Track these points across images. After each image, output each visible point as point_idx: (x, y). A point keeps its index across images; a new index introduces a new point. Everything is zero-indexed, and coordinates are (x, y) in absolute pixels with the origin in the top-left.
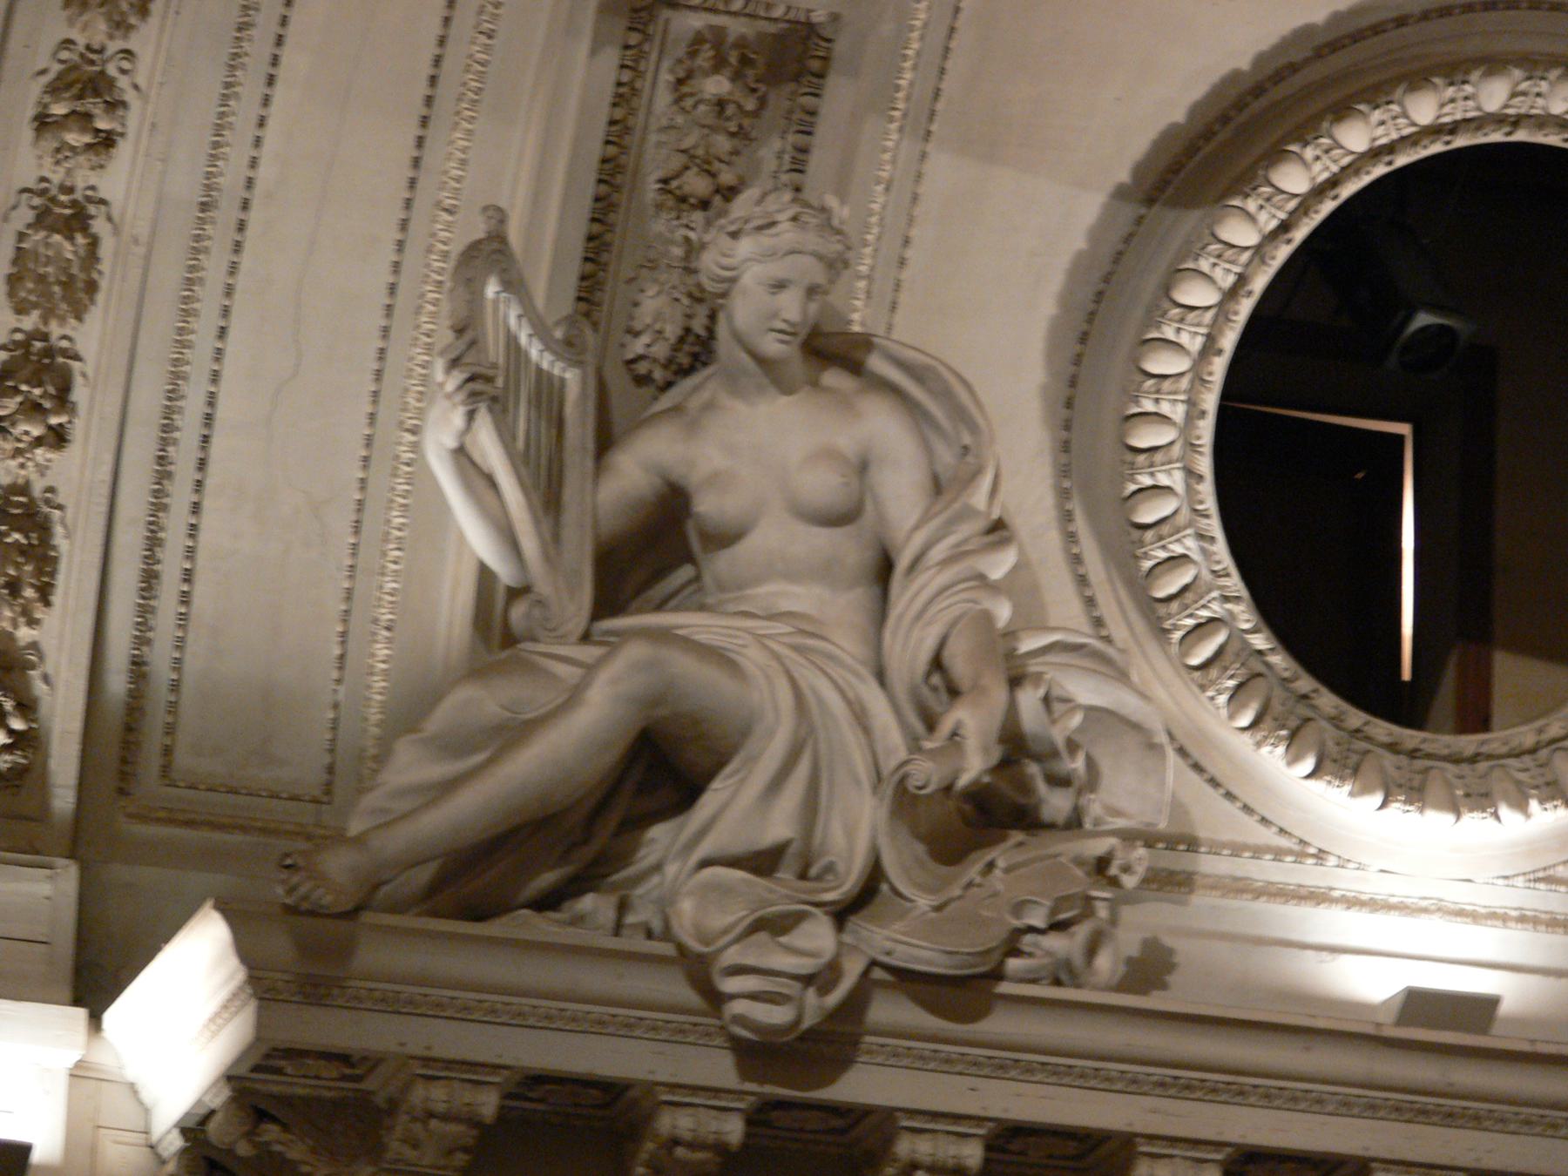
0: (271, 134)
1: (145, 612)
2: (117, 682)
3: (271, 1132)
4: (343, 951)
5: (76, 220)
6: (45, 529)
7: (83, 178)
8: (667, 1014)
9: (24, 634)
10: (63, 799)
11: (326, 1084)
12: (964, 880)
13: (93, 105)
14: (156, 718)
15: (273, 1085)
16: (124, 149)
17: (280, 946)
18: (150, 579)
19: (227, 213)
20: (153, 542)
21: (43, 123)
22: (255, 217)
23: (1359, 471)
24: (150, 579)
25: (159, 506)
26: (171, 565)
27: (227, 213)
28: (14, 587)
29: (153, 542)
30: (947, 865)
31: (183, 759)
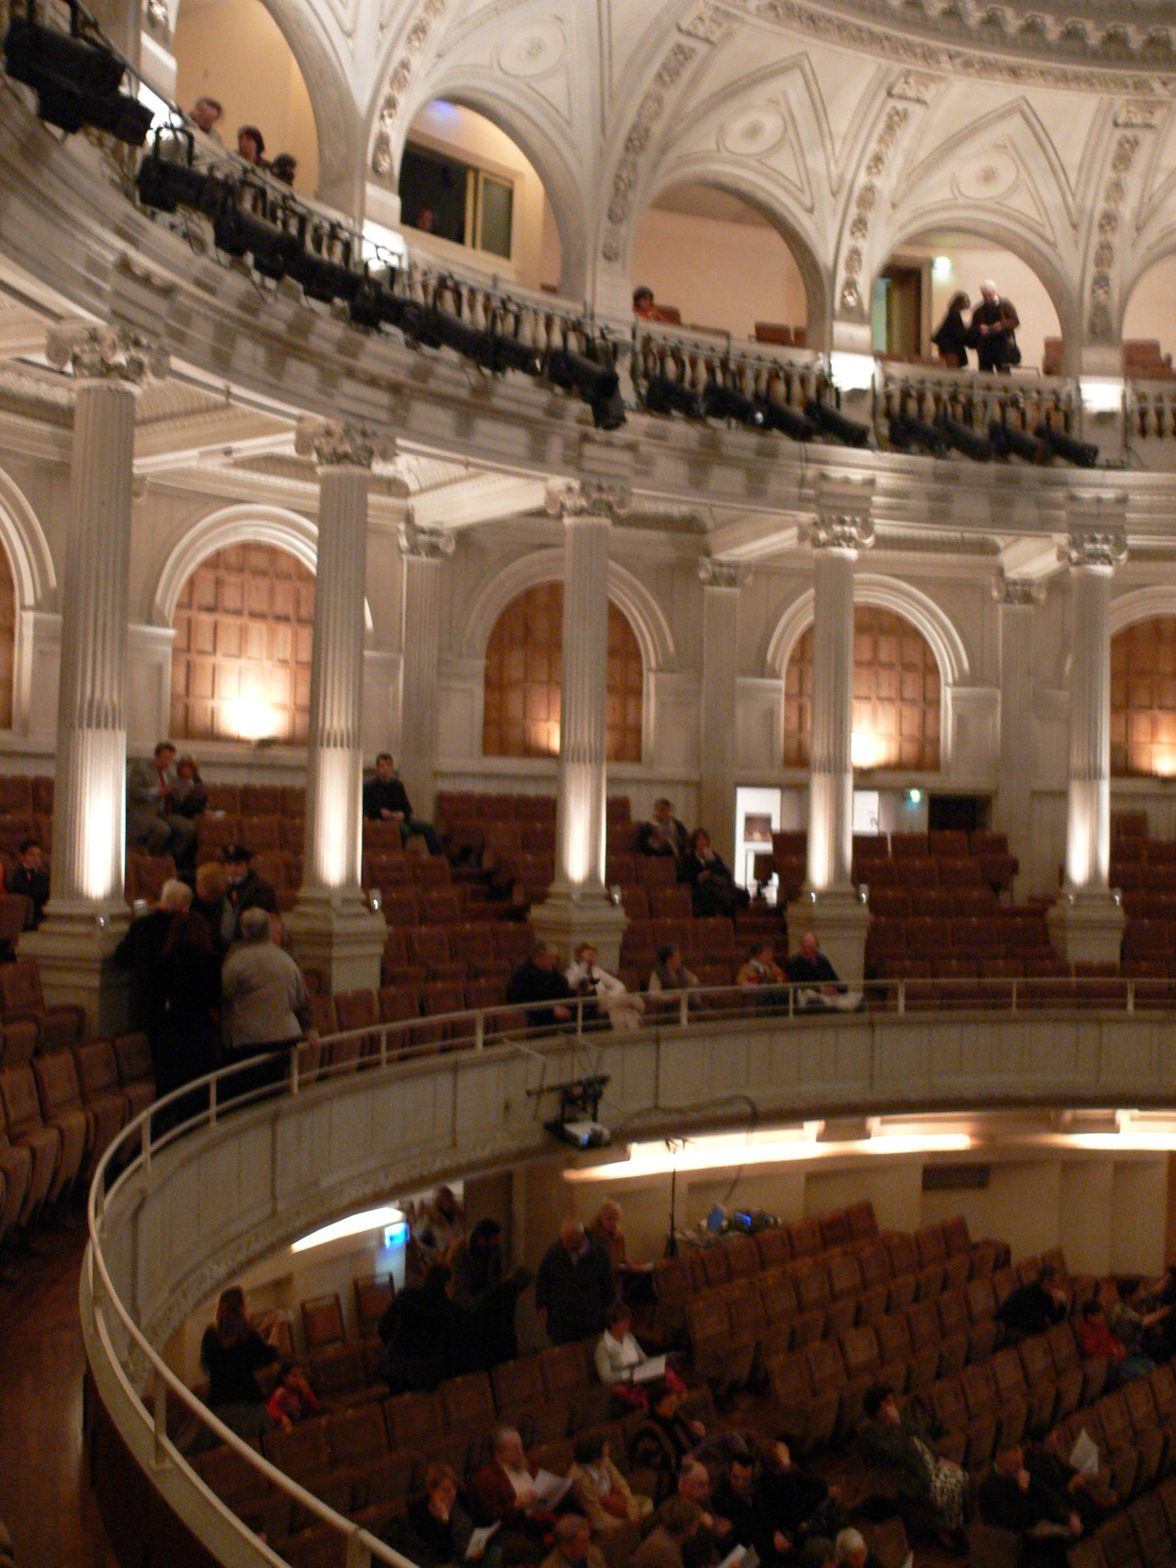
23: (1083, 1521)
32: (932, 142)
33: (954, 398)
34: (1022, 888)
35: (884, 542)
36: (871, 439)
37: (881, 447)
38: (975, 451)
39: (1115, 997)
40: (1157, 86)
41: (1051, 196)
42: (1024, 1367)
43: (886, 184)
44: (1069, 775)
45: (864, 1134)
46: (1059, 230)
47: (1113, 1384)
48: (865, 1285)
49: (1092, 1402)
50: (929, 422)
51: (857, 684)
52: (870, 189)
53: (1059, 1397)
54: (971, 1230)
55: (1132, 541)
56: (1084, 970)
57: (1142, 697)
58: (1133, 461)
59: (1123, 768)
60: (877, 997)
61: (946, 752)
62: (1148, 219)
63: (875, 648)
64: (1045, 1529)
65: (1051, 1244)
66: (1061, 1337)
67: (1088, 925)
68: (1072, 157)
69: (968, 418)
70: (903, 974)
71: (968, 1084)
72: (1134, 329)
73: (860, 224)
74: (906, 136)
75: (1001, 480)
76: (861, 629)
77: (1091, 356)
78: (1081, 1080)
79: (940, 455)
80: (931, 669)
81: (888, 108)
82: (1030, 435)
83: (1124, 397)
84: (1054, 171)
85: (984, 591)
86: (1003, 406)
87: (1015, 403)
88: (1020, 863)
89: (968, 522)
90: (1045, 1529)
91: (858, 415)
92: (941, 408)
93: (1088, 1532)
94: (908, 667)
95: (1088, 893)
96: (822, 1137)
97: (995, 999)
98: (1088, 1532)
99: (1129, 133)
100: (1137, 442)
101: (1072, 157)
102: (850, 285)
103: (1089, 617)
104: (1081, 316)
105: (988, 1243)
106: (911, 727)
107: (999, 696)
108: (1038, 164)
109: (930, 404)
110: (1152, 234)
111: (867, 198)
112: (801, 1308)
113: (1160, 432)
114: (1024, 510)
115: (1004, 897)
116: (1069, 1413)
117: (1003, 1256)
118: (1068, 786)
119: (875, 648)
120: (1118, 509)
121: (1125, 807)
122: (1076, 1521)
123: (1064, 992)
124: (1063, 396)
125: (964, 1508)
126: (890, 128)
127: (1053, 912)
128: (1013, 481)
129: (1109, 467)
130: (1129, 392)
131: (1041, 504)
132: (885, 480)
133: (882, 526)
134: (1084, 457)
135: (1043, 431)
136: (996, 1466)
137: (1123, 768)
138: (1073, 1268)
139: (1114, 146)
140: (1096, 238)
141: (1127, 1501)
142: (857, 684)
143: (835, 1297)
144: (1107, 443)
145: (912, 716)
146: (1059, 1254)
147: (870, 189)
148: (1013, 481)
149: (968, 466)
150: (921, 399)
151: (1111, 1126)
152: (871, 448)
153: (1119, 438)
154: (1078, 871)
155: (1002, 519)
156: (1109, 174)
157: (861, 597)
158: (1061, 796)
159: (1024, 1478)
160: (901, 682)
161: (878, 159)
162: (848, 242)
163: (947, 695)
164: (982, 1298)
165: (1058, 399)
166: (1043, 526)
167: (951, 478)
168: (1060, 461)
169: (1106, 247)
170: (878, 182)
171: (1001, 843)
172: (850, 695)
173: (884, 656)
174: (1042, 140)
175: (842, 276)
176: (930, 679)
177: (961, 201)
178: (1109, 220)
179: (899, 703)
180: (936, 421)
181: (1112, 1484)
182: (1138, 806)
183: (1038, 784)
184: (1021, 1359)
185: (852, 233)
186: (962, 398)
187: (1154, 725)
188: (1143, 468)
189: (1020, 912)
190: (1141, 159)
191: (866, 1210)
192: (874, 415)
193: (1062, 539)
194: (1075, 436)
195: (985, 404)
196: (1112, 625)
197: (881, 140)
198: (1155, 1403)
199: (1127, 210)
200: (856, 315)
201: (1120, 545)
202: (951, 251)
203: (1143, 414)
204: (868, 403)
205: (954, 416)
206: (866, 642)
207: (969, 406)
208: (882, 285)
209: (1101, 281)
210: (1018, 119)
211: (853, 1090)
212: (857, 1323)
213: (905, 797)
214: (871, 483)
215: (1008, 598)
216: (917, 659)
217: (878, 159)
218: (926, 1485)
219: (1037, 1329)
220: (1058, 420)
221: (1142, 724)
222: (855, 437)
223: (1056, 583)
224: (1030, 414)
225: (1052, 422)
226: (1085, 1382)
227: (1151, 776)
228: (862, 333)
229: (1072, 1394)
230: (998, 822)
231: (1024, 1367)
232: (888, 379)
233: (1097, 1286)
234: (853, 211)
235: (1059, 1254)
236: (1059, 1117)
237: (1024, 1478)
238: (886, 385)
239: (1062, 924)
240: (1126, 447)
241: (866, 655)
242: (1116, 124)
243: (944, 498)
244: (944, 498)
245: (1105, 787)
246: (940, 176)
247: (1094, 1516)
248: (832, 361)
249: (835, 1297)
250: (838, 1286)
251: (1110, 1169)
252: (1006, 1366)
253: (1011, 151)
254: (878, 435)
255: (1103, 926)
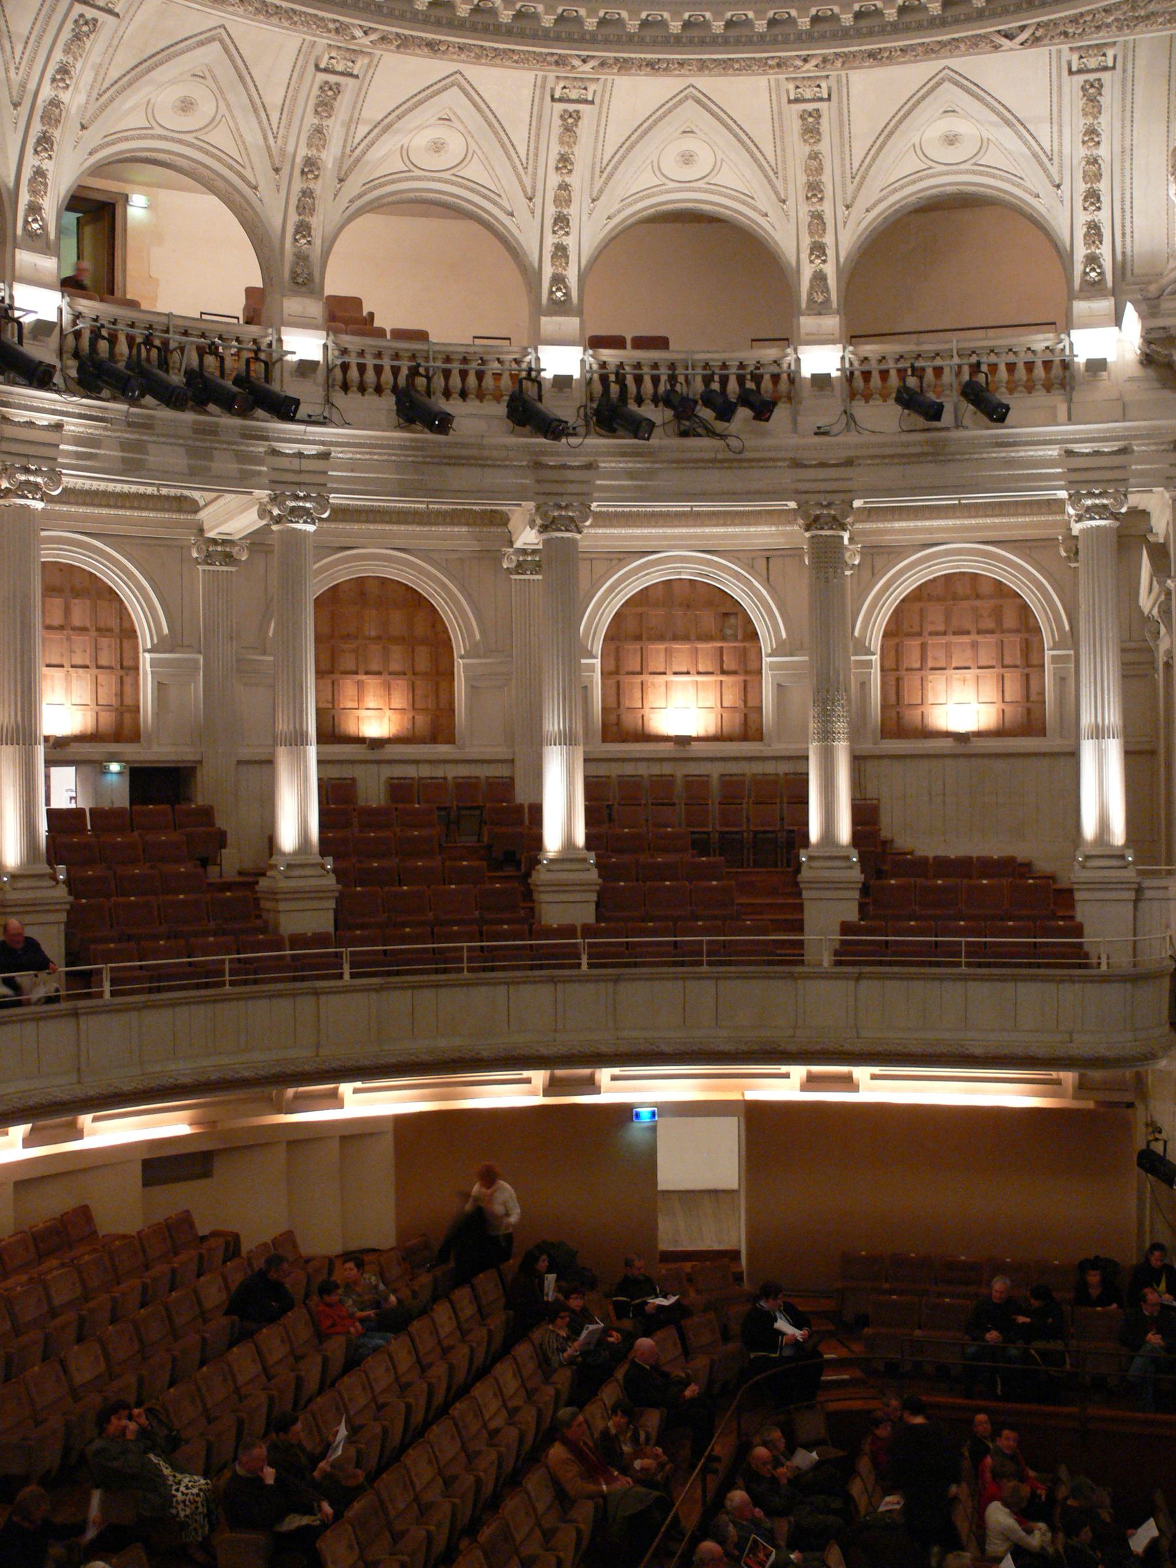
0: (1135, 133)
1: (1124, 242)
2: (1119, 257)
3: (1153, 346)
4: (1157, 307)
5: (1095, 161)
6: (1099, 229)
7: (1095, 152)
8: (151, 1130)
9: (1098, 251)
10: (1110, 284)
11: (1161, 334)
12: (1000, 744)
13: (1094, 136)
14: (1129, 263)
15: (1150, 336)
16: (1102, 144)
17: (1144, 307)
18: (1124, 234)
19: (1128, 152)
20: (1123, 226)
21: (1084, 142)
22: (1135, 152)
23: (331, 1505)
24: (1124, 234)
25: (1123, 218)
26: (1128, 230)
27: (1128, 152)
28: (1094, 242)
29: (1123, 226)
30: (38, 945)
31: (1136, 271)
32: (123, 61)
33: (148, 341)
34: (231, 861)
35: (70, 496)
36: (57, 379)
37: (68, 391)
38: (171, 398)
39: (329, 967)
40: (358, 33)
41: (252, 134)
42: (262, 1359)
43: (74, 99)
44: (275, 741)
45: (78, 1135)
46: (261, 173)
47: (353, 1362)
48: (86, 1298)
49: (333, 1384)
50: (121, 365)
51: (46, 648)
52: (55, 103)
53: (299, 1381)
54: (198, 1225)
55: (335, 499)
56: (298, 941)
57: (348, 662)
58: (336, 417)
59: (330, 734)
60: (82, 983)
61: (146, 722)
62: (350, 170)
63: (67, 611)
64: (295, 1522)
65: (283, 1228)
66: (297, 1322)
67: (297, 895)
68: (274, 97)
69: (164, 364)
70: (107, 958)
71: (183, 1069)
72: (336, 284)
73: (45, 142)
74: (96, 46)
75: (201, 431)
76: (50, 590)
77: (293, 305)
78: (301, 1055)
79: (133, 402)
80: (128, 633)
81: (74, 14)
82: (228, 383)
83: (325, 347)
84: (255, 110)
85: (183, 549)
86: (201, 351)
87: (213, 349)
88: (229, 836)
89: (165, 474)
90: (295, 1522)
91: (43, 352)
92: (134, 351)
93: (338, 1516)
94: (102, 631)
95: (297, 862)
96: (28, 1142)
97: (207, 978)
98: (338, 1516)
99: (333, 79)
100: (339, 398)
101: (274, 97)
102: (34, 209)
103: (292, 579)
104: (283, 265)
105: (215, 1234)
106: (107, 695)
107: (201, 657)
108: (238, 98)
109: (123, 347)
110: (353, 186)
111: (53, 112)
112: (17, 1331)
113: (362, 389)
114: (224, 464)
115: (213, 871)
116: (310, 1400)
117: (232, 1244)
118: (273, 754)
119: (67, 611)
120: (319, 465)
121: (335, 772)
122: (327, 1508)
123: (278, 965)
124: (263, 347)
125: (208, 1515)
126: (77, 37)
127: (264, 883)
128: (212, 431)
129: (310, 421)
130: (331, 345)
131: (244, 457)
132: (73, 426)
133: (72, 480)
134: (285, 409)
135: (242, 381)
136: (238, 1468)
137: (330, 734)
138: (305, 1250)
139: (315, 91)
140: (298, 185)
141: (373, 1477)
142: (46, 648)
143: (53, 1313)
144: (309, 395)
145: (109, 682)
146: (288, 1237)
147: (55, 103)
148: (212, 431)
149: (165, 414)
150: (113, 340)
151: (334, 1099)
152: (58, 392)
153: (321, 392)
154: (288, 839)
155: (199, 474)
156: (311, 120)
157: (48, 555)
158: (269, 763)
159: (269, 1475)
160: (97, 649)
161: (64, 70)
162: (31, 161)
163: (146, 659)
164: (213, 1294)
165: (258, 351)
166: (243, 481)
167: (146, 426)
168: (260, 413)
169: (307, 193)
170: (65, 97)
171: (207, 814)
172: (40, 660)
173: (77, 621)
174: (243, 74)
175: (24, 198)
176: (127, 644)
177: (158, 131)
178: (311, 166)
179: (95, 671)
180: (128, 366)
181: (358, 1465)
182: (347, 772)
183: (245, 753)
184: (259, 1353)
185: (36, 152)
186: (157, 342)
187: (360, 685)
188: (347, 424)
189: (228, 886)
190: (343, 105)
191: (84, 1213)
192: (61, 353)
193: (263, 494)
194: (275, 387)
195: (182, 349)
196: (316, 587)
197: (67, 50)
198: (396, 1373)
199: (329, 157)
200: (38, 242)
201: (322, 501)
202: (148, 186)
203: (345, 367)
204: (54, 340)
205: (148, 360)
206: (57, 603)
207: (165, 349)
208: (72, 218)
209: (303, 229)
210: (216, 45)
211: (61, 1087)
212: (80, 1339)
213: (105, 771)
214: (59, 427)
215: (208, 558)
216: (113, 623)
217: (64, 70)
218: (168, 1500)
219: (272, 1318)
220: (258, 369)
221: (348, 686)
222: (40, 377)
223: (257, 541)
224: (229, 363)
225: (252, 374)
226: (325, 1361)
227: (361, 740)
228: (48, 264)
229: (312, 1372)
230: (203, 793)
231: (262, 1359)
232: (78, 316)
233: (331, 1263)
234: (37, 128)
235: (288, 1237)
236: (280, 1095)
237: (269, 1475)
238: (75, 324)
239: (273, 894)
240: (328, 401)
241: (57, 619)
242: (317, 68)
243: (138, 447)
244: (139, 446)
245: (312, 751)
246: (134, 98)
247: (343, 1497)
248: (15, 293)
249: (53, 1313)
250: (57, 1301)
251: (336, 1144)
252: (244, 1362)
253: (210, 81)
254: (66, 378)
255: (316, 894)
